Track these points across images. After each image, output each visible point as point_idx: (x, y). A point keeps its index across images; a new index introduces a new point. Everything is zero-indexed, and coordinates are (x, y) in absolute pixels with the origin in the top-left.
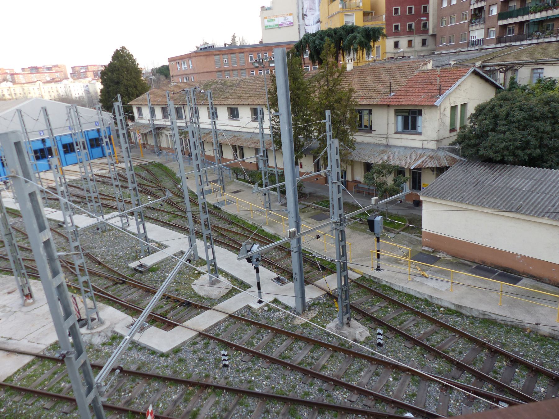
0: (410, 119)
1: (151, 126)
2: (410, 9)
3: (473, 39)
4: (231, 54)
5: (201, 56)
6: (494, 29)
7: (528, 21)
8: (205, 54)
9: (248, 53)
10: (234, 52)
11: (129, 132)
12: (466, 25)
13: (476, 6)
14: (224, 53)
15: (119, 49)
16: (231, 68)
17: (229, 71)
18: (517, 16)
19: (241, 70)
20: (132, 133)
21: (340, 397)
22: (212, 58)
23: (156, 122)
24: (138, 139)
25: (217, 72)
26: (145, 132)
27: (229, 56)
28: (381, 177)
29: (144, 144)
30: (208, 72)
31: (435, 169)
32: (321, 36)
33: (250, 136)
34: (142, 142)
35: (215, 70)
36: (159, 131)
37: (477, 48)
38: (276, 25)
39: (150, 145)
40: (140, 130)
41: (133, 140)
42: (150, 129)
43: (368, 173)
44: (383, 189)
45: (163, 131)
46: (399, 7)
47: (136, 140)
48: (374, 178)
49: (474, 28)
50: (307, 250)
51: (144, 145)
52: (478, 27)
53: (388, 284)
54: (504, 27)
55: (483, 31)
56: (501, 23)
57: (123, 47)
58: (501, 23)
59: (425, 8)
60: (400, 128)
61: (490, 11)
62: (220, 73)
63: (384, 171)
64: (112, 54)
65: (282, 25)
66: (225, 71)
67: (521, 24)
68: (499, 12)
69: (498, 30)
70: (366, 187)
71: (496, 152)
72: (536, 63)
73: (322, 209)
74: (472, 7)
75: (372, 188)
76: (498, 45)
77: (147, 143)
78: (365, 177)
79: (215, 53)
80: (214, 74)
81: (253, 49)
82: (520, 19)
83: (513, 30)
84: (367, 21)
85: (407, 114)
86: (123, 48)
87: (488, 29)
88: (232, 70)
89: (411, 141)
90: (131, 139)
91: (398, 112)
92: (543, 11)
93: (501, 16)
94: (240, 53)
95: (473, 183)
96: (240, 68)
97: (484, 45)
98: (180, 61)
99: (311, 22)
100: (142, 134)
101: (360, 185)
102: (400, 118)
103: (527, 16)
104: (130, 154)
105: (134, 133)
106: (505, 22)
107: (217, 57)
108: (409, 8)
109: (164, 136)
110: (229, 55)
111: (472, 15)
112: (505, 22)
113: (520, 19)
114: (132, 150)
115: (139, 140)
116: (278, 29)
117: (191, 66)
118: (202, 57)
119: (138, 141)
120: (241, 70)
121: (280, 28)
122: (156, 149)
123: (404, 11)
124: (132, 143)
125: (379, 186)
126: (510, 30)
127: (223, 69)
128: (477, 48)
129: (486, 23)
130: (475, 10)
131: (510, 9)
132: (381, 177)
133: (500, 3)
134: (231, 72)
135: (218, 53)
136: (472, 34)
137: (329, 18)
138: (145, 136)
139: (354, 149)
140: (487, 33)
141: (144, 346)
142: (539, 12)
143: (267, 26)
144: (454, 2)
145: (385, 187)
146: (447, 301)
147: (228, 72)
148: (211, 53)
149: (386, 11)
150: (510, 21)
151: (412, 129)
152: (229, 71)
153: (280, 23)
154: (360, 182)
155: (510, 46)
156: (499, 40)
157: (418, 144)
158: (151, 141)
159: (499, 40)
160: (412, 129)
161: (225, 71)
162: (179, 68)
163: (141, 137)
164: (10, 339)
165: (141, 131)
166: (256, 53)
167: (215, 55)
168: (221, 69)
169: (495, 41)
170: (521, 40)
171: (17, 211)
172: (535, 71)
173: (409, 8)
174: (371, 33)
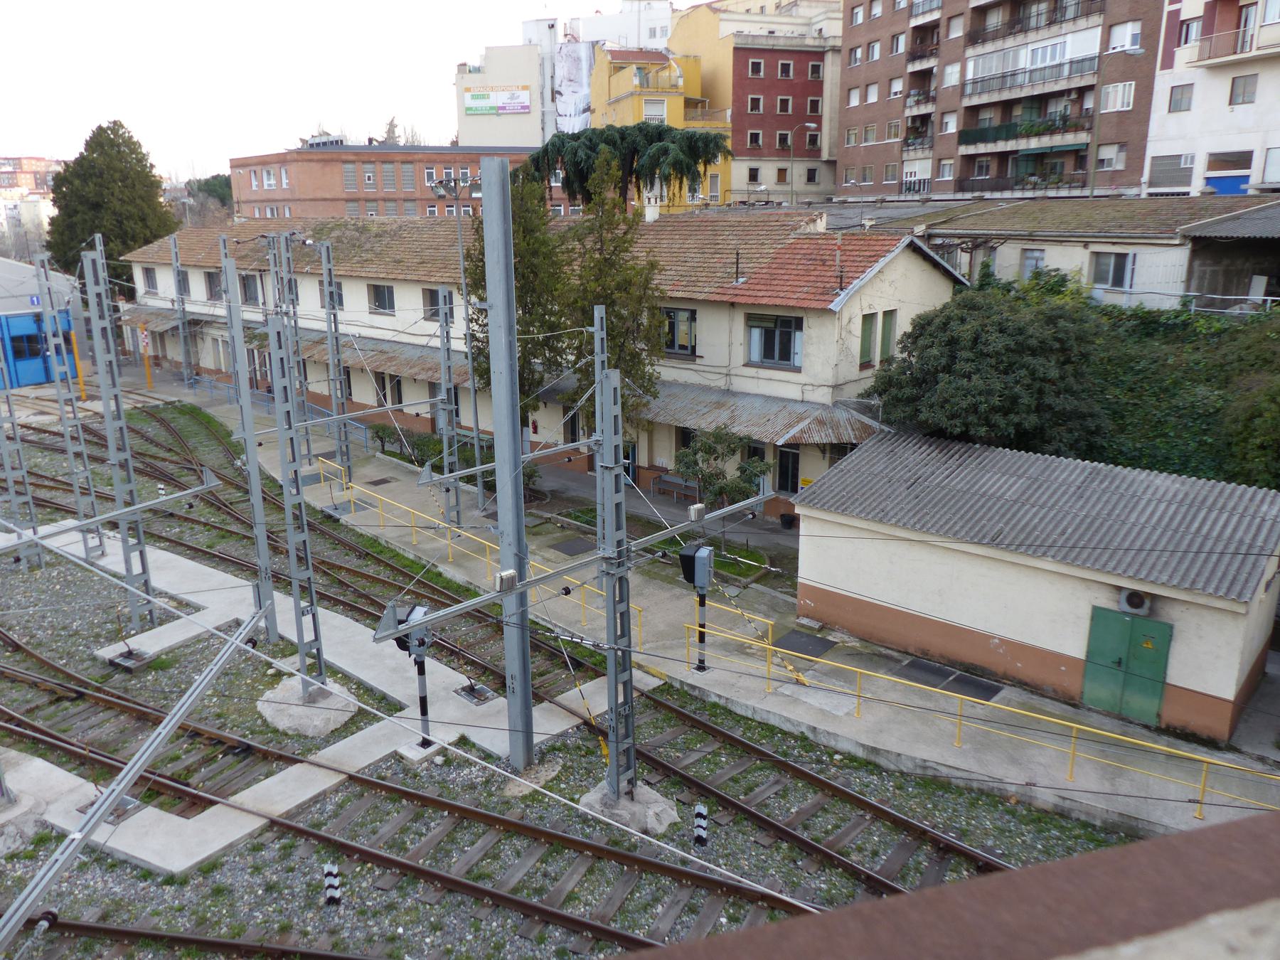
0: (777, 337)
1: (178, 315)
2: (784, 103)
4: (384, 162)
6: (952, 162)
8: (320, 157)
10: (390, 158)
11: (120, 327)
12: (896, 149)
13: (916, 111)
14: (366, 158)
15: (105, 125)
16: (382, 195)
17: (375, 200)
18: (995, 140)
19: (405, 200)
20: (127, 331)
23: (189, 308)
24: (142, 345)
25: (347, 200)
26: (160, 329)
27: (379, 167)
28: (712, 461)
29: (156, 357)
32: (591, 140)
33: (418, 353)
34: (150, 352)
35: (344, 196)
36: (198, 328)
37: (917, 197)
38: (491, 108)
39: (170, 362)
40: (146, 322)
41: (129, 345)
42: (174, 324)
43: (683, 450)
44: (717, 487)
45: (205, 330)
46: (762, 97)
47: (136, 345)
48: (696, 463)
49: (912, 154)
51: (157, 361)
52: (920, 154)
53: (722, 702)
54: (970, 159)
57: (115, 123)
59: (815, 105)
60: (756, 355)
61: (943, 125)
63: (719, 448)
65: (504, 108)
66: (367, 200)
67: (1003, 157)
69: (959, 164)
70: (680, 481)
74: (908, 113)
75: (693, 484)
76: (959, 196)
77: (165, 357)
78: (679, 460)
79: (344, 157)
80: (341, 205)
81: (435, 157)
84: (693, 119)
85: (772, 325)
86: (116, 125)
87: (940, 160)
88: (384, 200)
90: (123, 343)
91: (752, 320)
93: (965, 137)
94: (403, 162)
96: (402, 196)
98: (258, 168)
99: (571, 110)
100: (153, 333)
101: (666, 478)
102: (756, 334)
104: (119, 380)
105: (133, 331)
109: (209, 341)
110: (359, 165)
111: (908, 128)
114: (124, 370)
115: (146, 347)
118: (313, 164)
119: (142, 351)
121: (498, 115)
122: (185, 372)
123: (770, 106)
124: (125, 353)
125: (707, 480)
128: (917, 197)
130: (914, 118)
132: (712, 461)
133: (962, 111)
135: (352, 158)
136: (907, 168)
138: (159, 338)
140: (937, 169)
145: (721, 482)
146: (848, 739)
147: (374, 204)
148: (335, 156)
149: (734, 101)
150: (982, 148)
152: (375, 200)
154: (666, 471)
156: (961, 185)
157: (792, 392)
158: (175, 352)
159: (961, 185)
161: (367, 200)
162: (254, 183)
163: (149, 340)
165: (151, 327)
166: (442, 166)
170: (993, 189)
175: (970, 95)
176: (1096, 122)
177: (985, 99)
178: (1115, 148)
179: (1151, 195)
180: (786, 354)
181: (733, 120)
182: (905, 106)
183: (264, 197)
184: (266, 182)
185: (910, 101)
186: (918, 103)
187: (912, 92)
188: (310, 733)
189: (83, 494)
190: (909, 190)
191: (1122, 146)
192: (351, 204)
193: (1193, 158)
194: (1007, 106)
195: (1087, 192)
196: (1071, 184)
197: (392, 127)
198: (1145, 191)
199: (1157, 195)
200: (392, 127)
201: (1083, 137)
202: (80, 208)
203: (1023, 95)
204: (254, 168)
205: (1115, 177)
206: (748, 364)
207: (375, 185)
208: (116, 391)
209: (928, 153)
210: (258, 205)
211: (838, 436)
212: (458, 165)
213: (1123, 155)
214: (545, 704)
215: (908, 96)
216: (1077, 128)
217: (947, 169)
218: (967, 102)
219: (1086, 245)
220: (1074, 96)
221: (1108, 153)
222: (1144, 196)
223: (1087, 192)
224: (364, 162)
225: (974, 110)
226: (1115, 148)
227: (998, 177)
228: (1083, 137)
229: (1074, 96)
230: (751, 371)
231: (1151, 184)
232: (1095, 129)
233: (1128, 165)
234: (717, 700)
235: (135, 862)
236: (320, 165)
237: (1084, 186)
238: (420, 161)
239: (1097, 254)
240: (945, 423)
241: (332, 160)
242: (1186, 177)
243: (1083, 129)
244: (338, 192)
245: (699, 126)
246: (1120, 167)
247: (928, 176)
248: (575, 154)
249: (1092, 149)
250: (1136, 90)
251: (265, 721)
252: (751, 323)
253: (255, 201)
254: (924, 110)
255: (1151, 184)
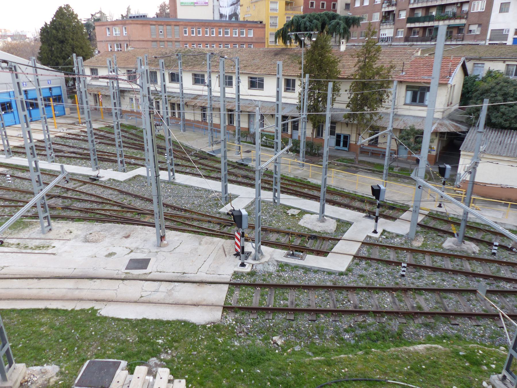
0: (419, 94)
2: (323, 4)
3: (382, 36)
4: (167, 25)
5: (137, 24)
6: (403, 30)
7: (433, 26)
8: (141, 22)
9: (183, 27)
10: (170, 24)
12: (377, 25)
13: (387, 9)
14: (160, 23)
15: (63, 6)
16: (166, 39)
17: (164, 41)
18: (424, 22)
19: (176, 42)
21: (371, 319)
22: (148, 27)
25: (152, 41)
27: (165, 27)
30: (144, 41)
31: (438, 134)
32: (309, 18)
33: (248, 102)
35: (151, 39)
37: (386, 44)
38: (192, 3)
46: (315, 2)
49: (385, 27)
50: (365, 196)
52: (388, 26)
53: (456, 217)
54: (410, 29)
55: (392, 30)
56: (409, 25)
57: (67, 5)
58: (409, 25)
59: (334, 5)
60: (409, 100)
61: (399, 15)
62: (155, 43)
64: (56, 9)
65: (197, 3)
66: (160, 41)
67: (425, 28)
68: (408, 16)
69: (406, 31)
71: (506, 120)
72: (480, 59)
73: (345, 165)
74: (383, 10)
76: (406, 43)
79: (151, 23)
80: (150, 43)
81: (187, 23)
82: (426, 24)
83: (418, 32)
84: (288, 10)
85: (417, 90)
86: (68, 6)
87: (397, 29)
88: (168, 41)
89: (418, 111)
91: (408, 88)
92: (446, 20)
93: (410, 20)
94: (175, 25)
95: (497, 142)
96: (175, 40)
97: (392, 41)
98: (110, 27)
99: (225, 5)
102: (409, 93)
103: (432, 23)
106: (412, 25)
107: (153, 27)
108: (322, 3)
110: (157, 26)
111: (383, 16)
112: (412, 25)
113: (426, 24)
116: (193, 7)
117: (124, 32)
118: (138, 26)
120: (176, 42)
121: (195, 6)
123: (317, 6)
126: (414, 33)
127: (158, 39)
128: (386, 44)
129: (396, 24)
130: (386, 12)
131: (415, 16)
133: (409, 10)
134: (166, 42)
135: (154, 23)
136: (382, 32)
137: (252, 3)
139: (184, 131)
140: (396, 33)
141: (316, 269)
142: (443, 20)
143: (182, 3)
144: (366, 3)
146: (510, 225)
147: (163, 43)
148: (147, 22)
149: (304, 3)
150: (417, 25)
151: (420, 102)
152: (164, 41)
153: (196, 2)
155: (413, 45)
156: (407, 39)
157: (424, 114)
159: (407, 39)
160: (420, 102)
161: (160, 41)
162: (108, 33)
164: (184, 273)
166: (190, 27)
167: (151, 25)
168: (157, 39)
169: (403, 39)
170: (422, 41)
171: (26, 167)
172: (476, 65)
173: (322, 3)
174: (351, 21)
175: (413, 4)
176: (469, 16)
177: (420, 5)
178: (477, 26)
179: (490, 44)
180: (422, 101)
181: (304, 11)
182: (382, 7)
183: (114, 39)
184: (114, 33)
185: (384, 5)
186: (388, 6)
187: (385, 2)
188: (329, 232)
189: (264, 145)
190: (383, 41)
191: (480, 25)
192: (153, 43)
193: (509, 30)
194: (428, 8)
195: (464, 43)
196: (457, 39)
197: (128, 10)
198: (488, 42)
199: (492, 44)
200: (128, 10)
201: (463, 21)
202: (55, 42)
203: (437, 4)
204: (108, 27)
205: (476, 37)
206: (405, 104)
207: (163, 35)
208: (90, 119)
209: (392, 26)
210: (111, 43)
211: (449, 129)
212: (197, 27)
213: (480, 29)
214: (398, 220)
215: (383, 3)
216: (461, 18)
217: (400, 33)
218: (411, 6)
219: (504, 62)
220: (459, 5)
221: (472, 28)
222: (487, 44)
223: (464, 43)
224: (159, 25)
225: (413, 10)
226: (477, 26)
227: (423, 36)
228: (463, 21)
229: (459, 5)
230: (407, 107)
231: (490, 40)
232: (468, 18)
233: (481, 32)
234: (453, 216)
235: (323, 270)
236: (141, 26)
237: (462, 40)
238: (182, 25)
239: (508, 65)
240: (503, 123)
241: (146, 24)
242: (506, 37)
243: (463, 18)
244: (149, 38)
245: (349, 14)
246: (478, 33)
247: (392, 35)
248: (305, 24)
249: (467, 26)
250: (486, 3)
251: (309, 229)
252: (408, 89)
253: (109, 41)
254: (390, 9)
255: (490, 40)
